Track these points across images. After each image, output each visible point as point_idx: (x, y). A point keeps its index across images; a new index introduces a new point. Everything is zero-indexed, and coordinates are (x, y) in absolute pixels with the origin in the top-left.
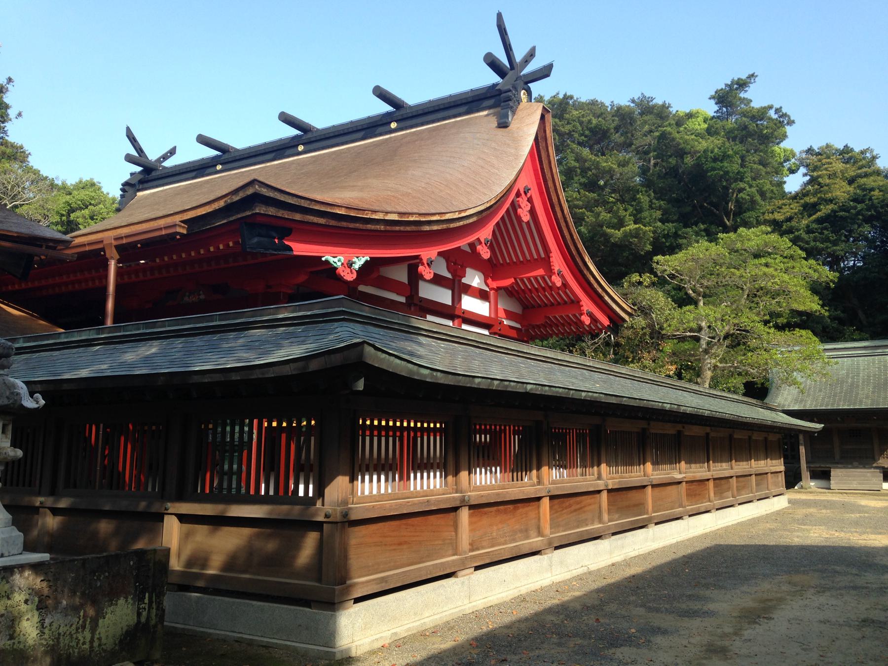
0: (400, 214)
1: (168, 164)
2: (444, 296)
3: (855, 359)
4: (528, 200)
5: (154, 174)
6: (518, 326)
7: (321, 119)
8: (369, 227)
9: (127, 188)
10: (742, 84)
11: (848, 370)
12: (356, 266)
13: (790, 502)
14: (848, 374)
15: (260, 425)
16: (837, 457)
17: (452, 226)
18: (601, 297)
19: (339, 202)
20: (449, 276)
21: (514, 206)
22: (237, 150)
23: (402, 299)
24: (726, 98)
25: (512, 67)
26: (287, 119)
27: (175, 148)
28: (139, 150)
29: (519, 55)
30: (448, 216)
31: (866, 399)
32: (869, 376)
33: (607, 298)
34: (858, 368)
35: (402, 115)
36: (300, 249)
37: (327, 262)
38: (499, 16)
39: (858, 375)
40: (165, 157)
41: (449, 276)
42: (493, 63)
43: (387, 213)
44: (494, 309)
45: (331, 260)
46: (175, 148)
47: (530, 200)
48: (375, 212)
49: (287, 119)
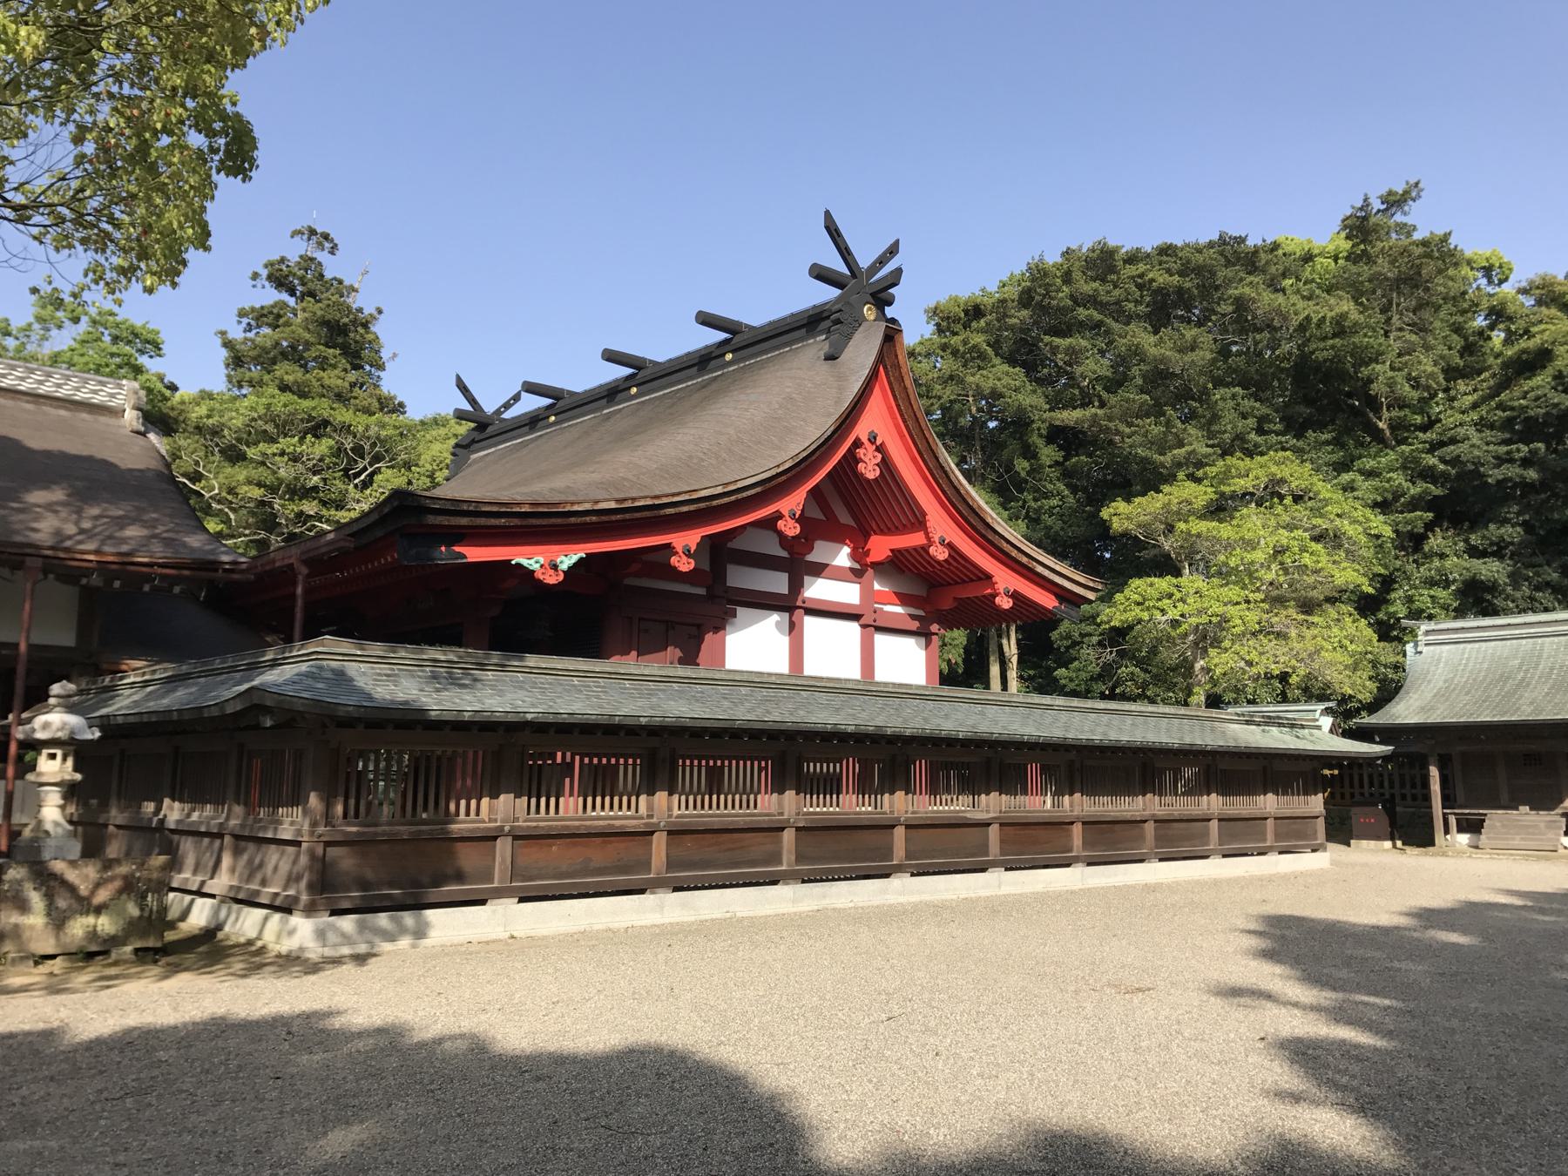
0: (617, 501)
1: (507, 415)
2: (777, 583)
3: (1540, 640)
4: (878, 449)
5: (490, 430)
6: (921, 613)
7: (757, 313)
8: (573, 520)
9: (458, 451)
10: (1395, 201)
11: (1523, 658)
12: (564, 567)
13: (1333, 862)
14: (1521, 665)
15: (582, 761)
16: (1505, 797)
17: (715, 503)
18: (1032, 570)
19: (519, 498)
20: (784, 554)
21: (851, 459)
22: (655, 363)
23: (701, 591)
24: (1360, 227)
25: (854, 275)
26: (706, 320)
27: (897, 243)
28: (472, 401)
29: (864, 260)
30: (740, 485)
31: (1535, 704)
32: (1552, 669)
33: (1040, 569)
34: (1540, 656)
35: (643, 376)
36: (475, 554)
37: (519, 565)
38: (459, 379)
39: (1536, 668)
40: (507, 406)
41: (784, 554)
42: (821, 274)
43: (597, 502)
44: (866, 593)
45: (525, 562)
46: (897, 243)
47: (880, 449)
48: (573, 504)
49: (706, 320)
